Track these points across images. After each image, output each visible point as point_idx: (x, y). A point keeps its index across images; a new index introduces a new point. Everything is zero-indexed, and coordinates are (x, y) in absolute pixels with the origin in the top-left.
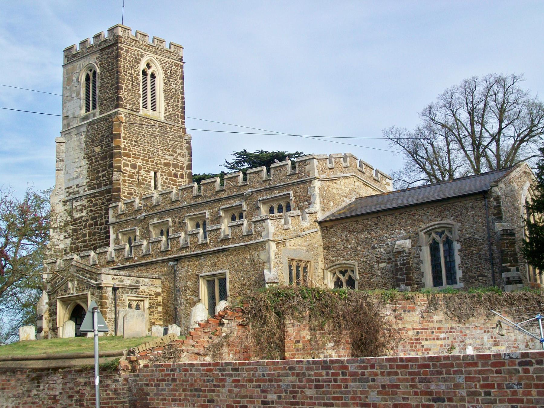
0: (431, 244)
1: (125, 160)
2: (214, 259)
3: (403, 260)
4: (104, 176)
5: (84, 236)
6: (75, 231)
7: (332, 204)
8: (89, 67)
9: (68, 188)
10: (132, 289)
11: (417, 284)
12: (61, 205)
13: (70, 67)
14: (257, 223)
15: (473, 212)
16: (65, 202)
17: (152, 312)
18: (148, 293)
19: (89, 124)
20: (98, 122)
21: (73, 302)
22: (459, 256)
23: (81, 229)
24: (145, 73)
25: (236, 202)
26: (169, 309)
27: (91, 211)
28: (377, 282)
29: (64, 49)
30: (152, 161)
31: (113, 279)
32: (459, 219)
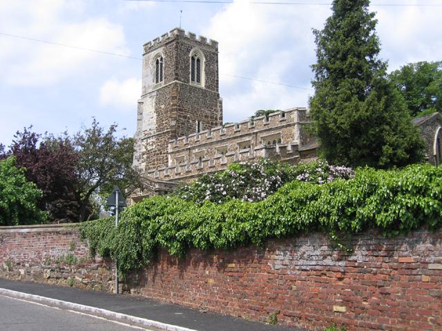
6: (148, 158)
19: (158, 91)
24: (193, 58)
25: (247, 139)
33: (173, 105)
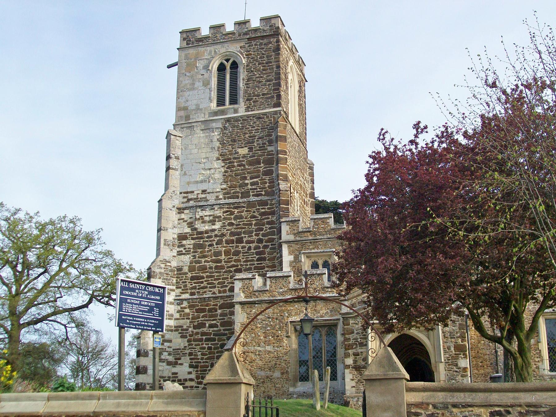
6: (196, 246)
8: (227, 56)
9: (187, 193)
12: (175, 213)
13: (192, 51)
16: (180, 210)
20: (243, 120)
27: (231, 224)
29: (181, 31)
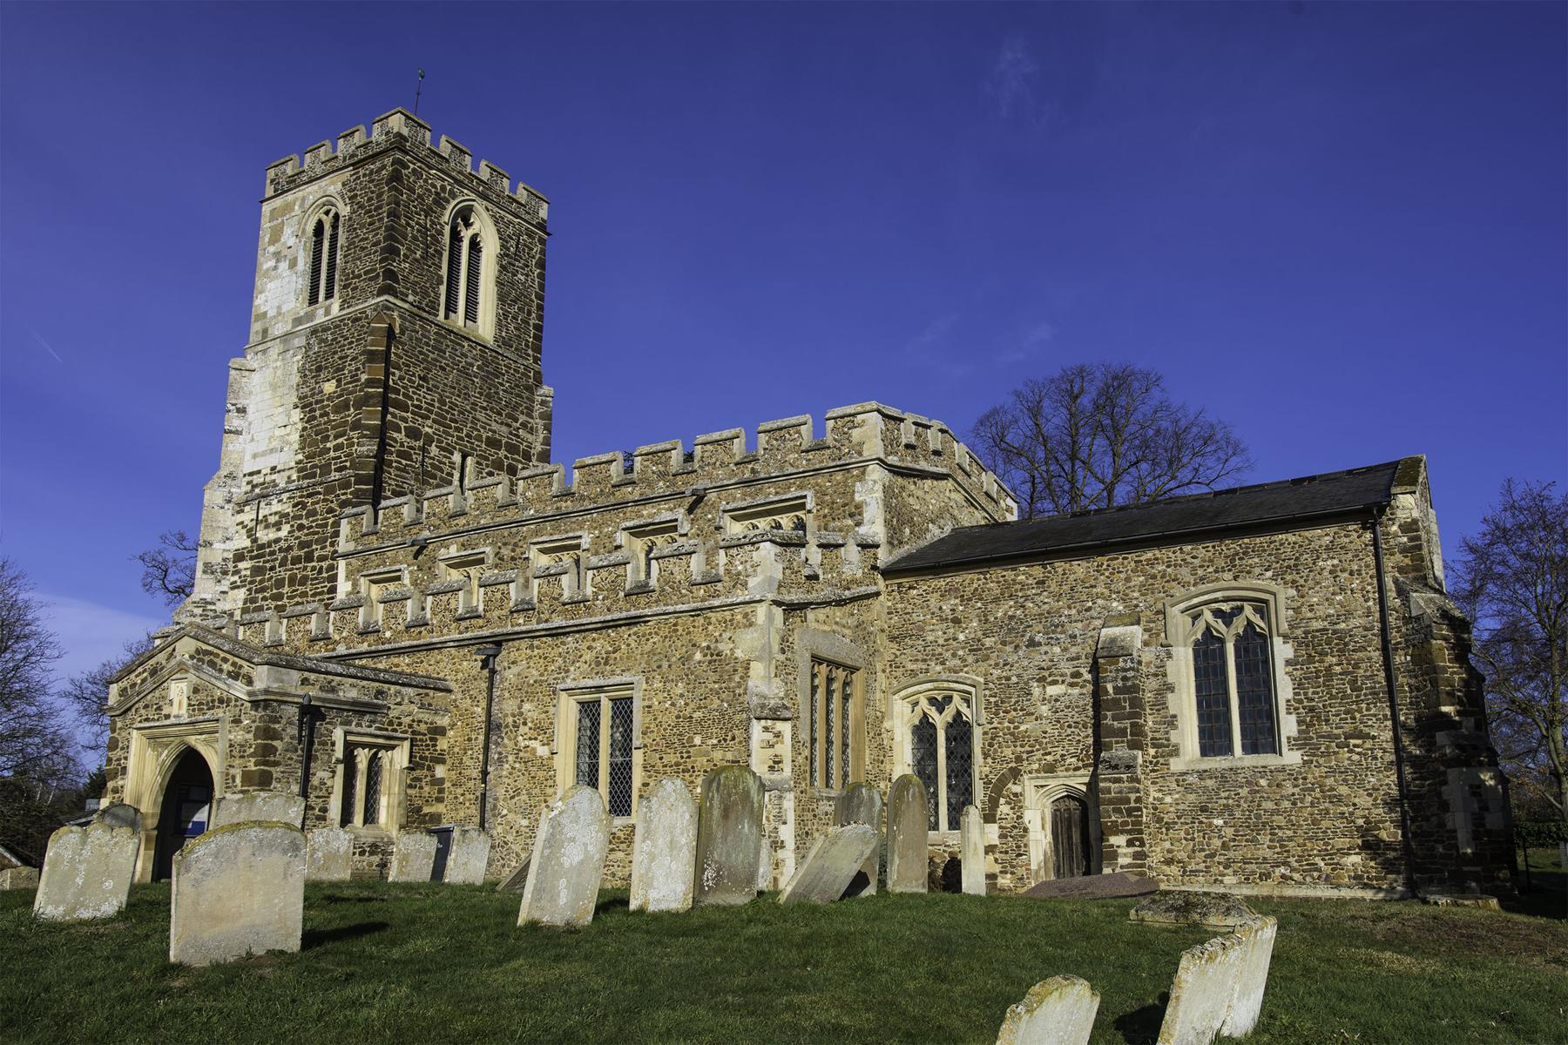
0: (1197, 643)
1: (394, 416)
2: (601, 644)
3: (1125, 679)
4: (337, 448)
5: (280, 583)
6: (257, 571)
7: (907, 531)
9: (251, 474)
10: (363, 713)
11: (1154, 746)
14: (733, 551)
15: (1336, 562)
17: (418, 779)
18: (410, 726)
19: (314, 332)
21: (177, 740)
22: (1287, 678)
23: (272, 569)
26: (467, 772)
28: (1039, 733)
30: (458, 430)
31: (305, 681)
32: (1288, 578)
33: (370, 383)
